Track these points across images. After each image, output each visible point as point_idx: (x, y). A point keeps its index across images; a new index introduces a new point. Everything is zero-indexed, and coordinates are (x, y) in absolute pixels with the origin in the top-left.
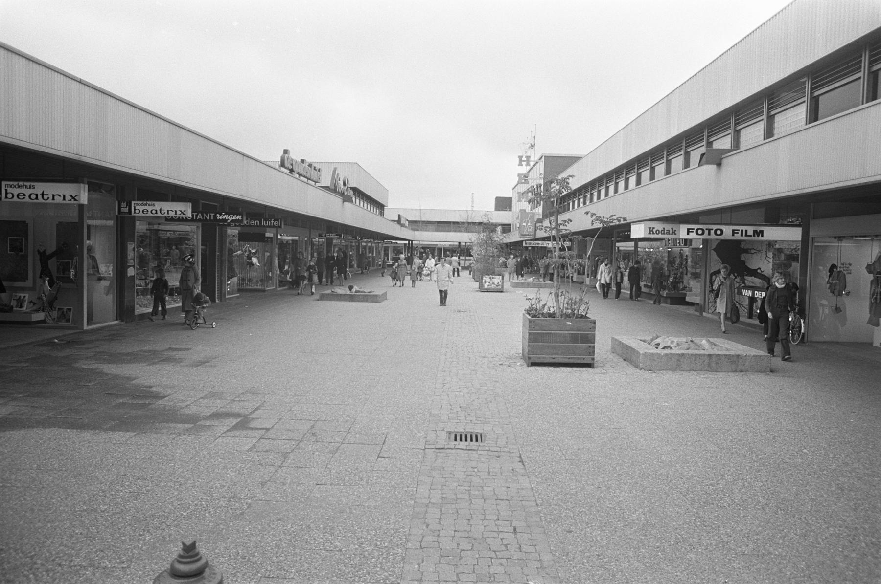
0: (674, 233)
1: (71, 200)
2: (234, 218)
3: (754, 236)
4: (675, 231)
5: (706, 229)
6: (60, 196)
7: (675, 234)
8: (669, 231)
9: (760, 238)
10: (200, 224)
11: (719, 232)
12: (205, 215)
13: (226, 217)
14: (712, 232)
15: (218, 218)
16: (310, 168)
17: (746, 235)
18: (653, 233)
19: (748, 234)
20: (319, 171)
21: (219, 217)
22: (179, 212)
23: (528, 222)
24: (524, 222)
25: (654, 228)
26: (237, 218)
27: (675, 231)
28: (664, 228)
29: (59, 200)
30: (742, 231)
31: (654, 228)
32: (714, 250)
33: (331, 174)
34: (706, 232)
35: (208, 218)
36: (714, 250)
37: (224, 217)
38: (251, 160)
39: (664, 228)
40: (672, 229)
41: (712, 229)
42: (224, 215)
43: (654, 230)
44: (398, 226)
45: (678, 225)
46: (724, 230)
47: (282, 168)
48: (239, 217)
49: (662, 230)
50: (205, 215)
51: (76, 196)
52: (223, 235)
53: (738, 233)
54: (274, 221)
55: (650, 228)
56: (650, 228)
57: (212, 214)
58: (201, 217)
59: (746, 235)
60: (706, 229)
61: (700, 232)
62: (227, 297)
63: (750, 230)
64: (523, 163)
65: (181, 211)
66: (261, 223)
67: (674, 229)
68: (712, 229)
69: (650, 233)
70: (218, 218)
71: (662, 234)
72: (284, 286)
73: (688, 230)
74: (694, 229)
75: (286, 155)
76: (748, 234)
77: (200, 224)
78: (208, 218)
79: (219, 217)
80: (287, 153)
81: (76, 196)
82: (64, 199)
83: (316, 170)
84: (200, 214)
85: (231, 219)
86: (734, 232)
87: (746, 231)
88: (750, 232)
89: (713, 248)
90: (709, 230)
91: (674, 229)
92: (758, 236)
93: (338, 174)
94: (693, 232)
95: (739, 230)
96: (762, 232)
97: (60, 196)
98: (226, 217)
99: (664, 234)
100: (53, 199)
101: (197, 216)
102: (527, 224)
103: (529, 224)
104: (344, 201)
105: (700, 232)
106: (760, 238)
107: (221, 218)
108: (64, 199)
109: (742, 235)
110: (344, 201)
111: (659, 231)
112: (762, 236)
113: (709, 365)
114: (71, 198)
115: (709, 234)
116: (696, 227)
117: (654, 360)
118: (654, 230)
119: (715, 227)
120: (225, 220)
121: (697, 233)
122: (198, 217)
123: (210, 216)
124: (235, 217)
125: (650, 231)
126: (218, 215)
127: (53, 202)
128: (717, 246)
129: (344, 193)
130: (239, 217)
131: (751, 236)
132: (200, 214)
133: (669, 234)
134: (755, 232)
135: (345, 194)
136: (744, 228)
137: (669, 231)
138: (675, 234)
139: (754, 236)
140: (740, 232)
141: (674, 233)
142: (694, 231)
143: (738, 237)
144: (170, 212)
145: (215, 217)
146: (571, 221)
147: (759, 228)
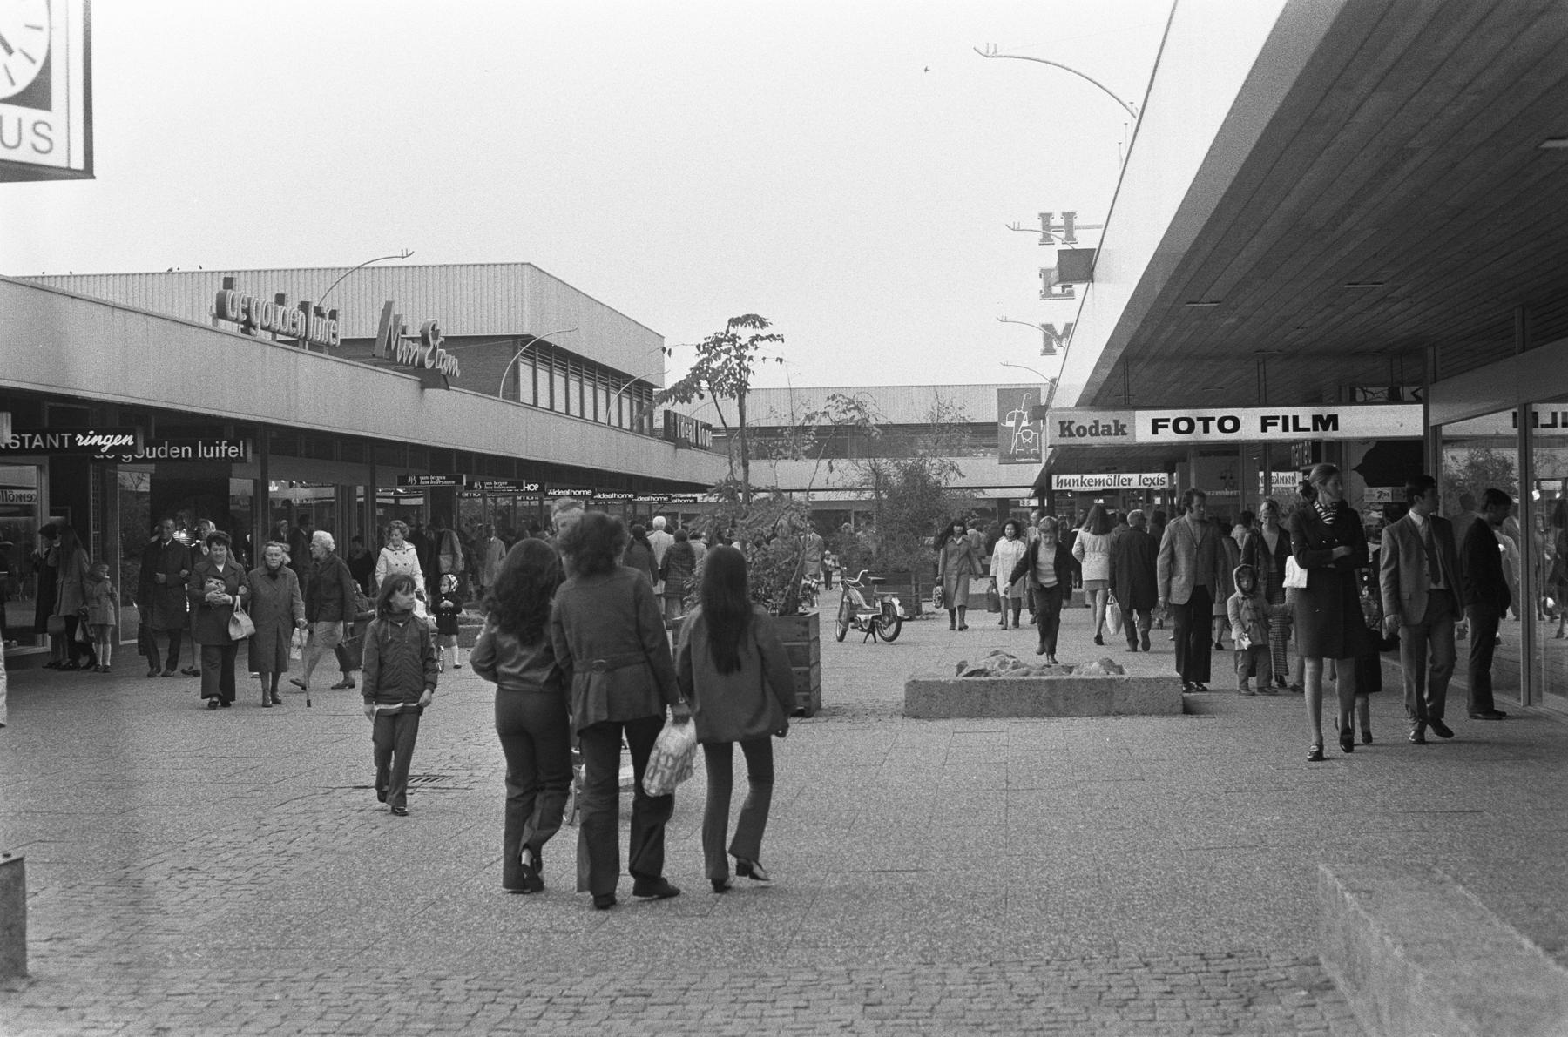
0: (1120, 430)
2: (116, 443)
4: (1124, 426)
5: (1199, 419)
8: (1109, 426)
10: (45, 460)
11: (1229, 425)
12: (49, 437)
13: (97, 440)
14: (1213, 425)
15: (80, 444)
16: (302, 314)
17: (1296, 428)
18: (1071, 435)
19: (1301, 425)
20: (333, 315)
21: (81, 441)
22: (292, 306)
23: (1021, 416)
24: (1011, 419)
25: (1071, 423)
26: (124, 442)
27: (1124, 426)
30: (1285, 419)
31: (1071, 423)
32: (1359, 469)
33: (378, 318)
34: (1199, 425)
35: (57, 445)
36: (1359, 469)
37: (93, 442)
39: (1096, 422)
40: (1116, 422)
41: (1213, 419)
42: (92, 436)
43: (1074, 428)
44: (665, 448)
46: (1242, 419)
47: (221, 321)
48: (128, 440)
49: (1091, 427)
50: (49, 437)
52: (108, 483)
53: (1275, 424)
54: (228, 445)
55: (1062, 423)
56: (1062, 423)
57: (27, 436)
58: (41, 443)
60: (1199, 419)
61: (1183, 426)
62: (121, 643)
63: (1305, 415)
64: (1061, 222)
66: (195, 451)
67: (1121, 422)
68: (1213, 419)
69: (1062, 435)
70: (80, 444)
71: (1092, 435)
73: (1155, 422)
74: (1168, 420)
75: (229, 291)
76: (1301, 425)
77: (45, 460)
78: (57, 445)
79: (81, 441)
80: (231, 288)
83: (323, 316)
84: (38, 436)
85: (109, 444)
86: (1156, 426)
87: (1296, 419)
88: (1306, 422)
89: (1354, 465)
90: (1206, 421)
91: (1121, 422)
92: (1325, 429)
93: (398, 318)
94: (1166, 427)
95: (1277, 418)
96: (1333, 419)
98: (97, 440)
99: (1097, 434)
101: (31, 440)
102: (1018, 423)
103: (1025, 423)
104: (424, 386)
105: (1183, 426)
107: (86, 443)
109: (1285, 429)
110: (424, 386)
111: (1084, 428)
112: (1335, 428)
113: (1050, 701)
115: (1206, 430)
116: (1172, 414)
117: (933, 696)
119: (1218, 413)
120: (97, 448)
121: (1176, 429)
122: (35, 443)
123: (62, 440)
124: (120, 440)
126: (79, 437)
128: (1366, 458)
129: (421, 364)
130: (128, 440)
131: (1307, 429)
132: (38, 436)
133: (1110, 434)
135: (428, 366)
136: (1290, 412)
139: (1315, 429)
140: (1280, 422)
142: (1170, 424)
143: (1275, 433)
145: (73, 441)
147: (1326, 411)
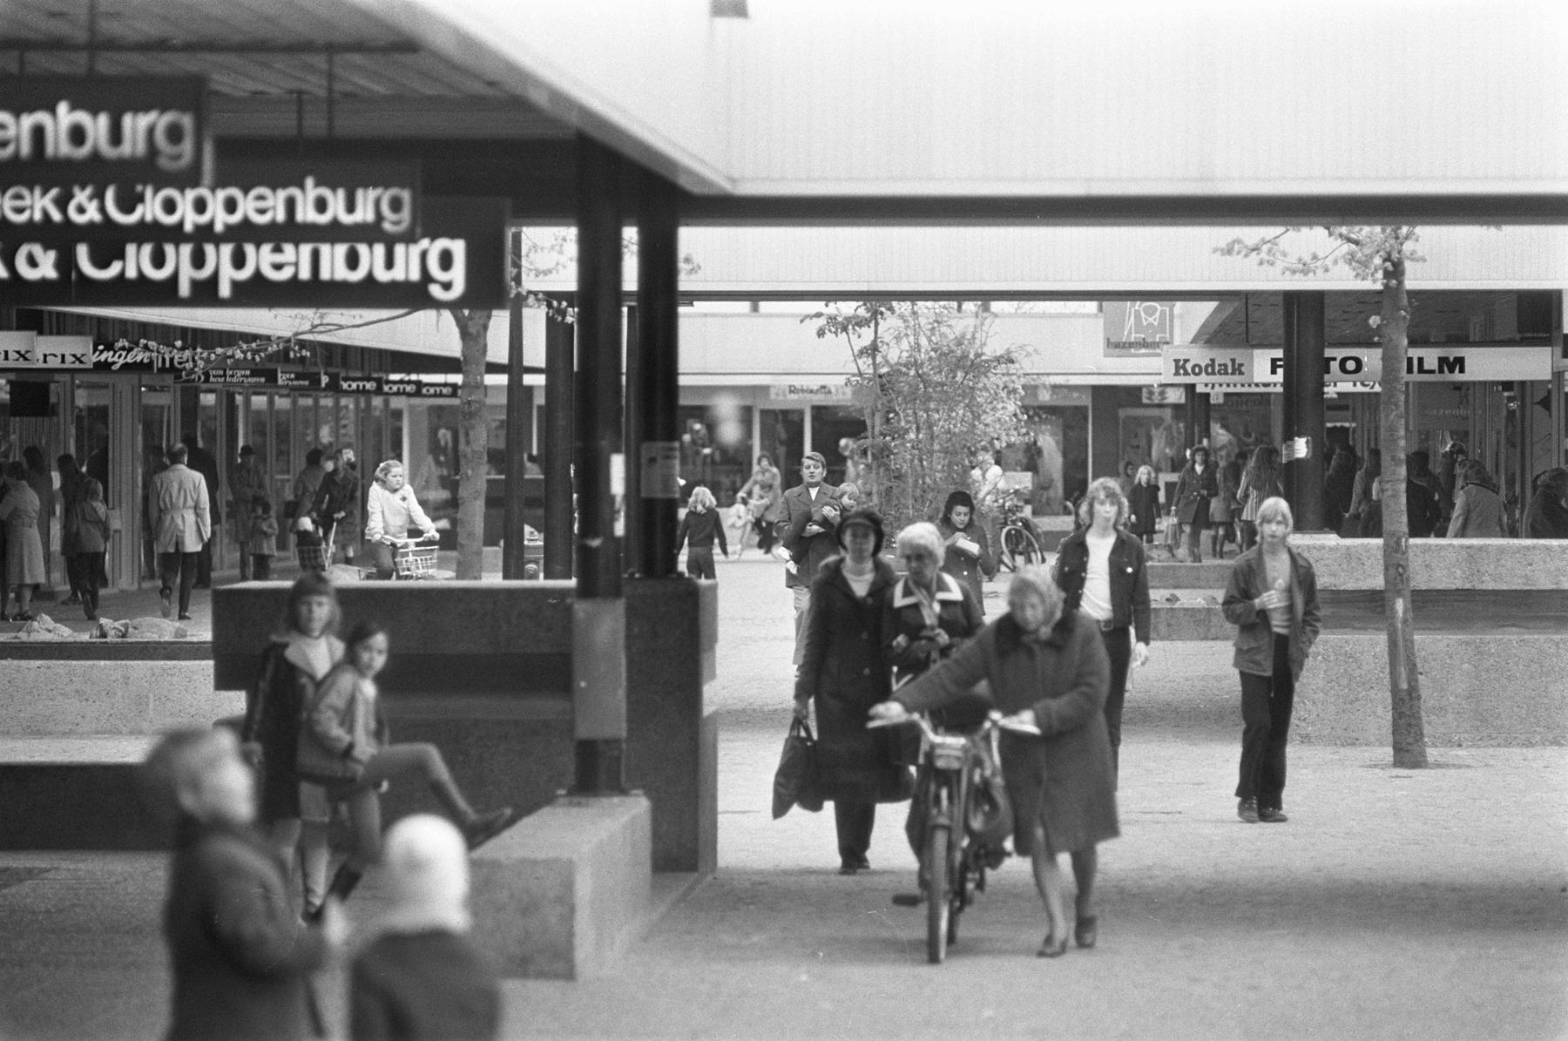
0: (1238, 369)
1: (74, 363)
2: (129, 360)
3: (1441, 371)
4: (1241, 365)
6: (55, 356)
7: (1241, 373)
8: (1225, 365)
9: (1457, 377)
11: (1351, 365)
17: (1421, 370)
18: (1186, 373)
19: (1426, 367)
25: (1186, 361)
27: (1241, 365)
28: (1213, 361)
29: (54, 363)
31: (1186, 361)
37: (103, 358)
38: (775, 320)
39: (1213, 361)
40: (1233, 361)
41: (1334, 359)
42: (101, 352)
43: (1189, 367)
45: (1249, 351)
49: (1207, 366)
51: (27, 352)
55: (1177, 361)
56: (1177, 361)
59: (1421, 370)
65: (74, 356)
68: (1334, 359)
69: (1177, 373)
71: (1207, 374)
72: (1134, 509)
76: (1426, 367)
81: (27, 352)
82: (63, 361)
85: (121, 361)
87: (1421, 360)
88: (1431, 362)
92: (1452, 371)
96: (1460, 361)
97: (55, 356)
99: (1213, 373)
100: (45, 361)
106: (1457, 377)
108: (63, 361)
112: (1462, 371)
114: (17, 356)
118: (1189, 367)
125: (1177, 368)
127: (45, 366)
131: (1432, 372)
133: (1226, 373)
134: (1443, 361)
137: (1225, 365)
138: (1241, 373)
139: (1441, 371)
141: (1238, 369)
144: (48, 358)
146: (859, 337)
147: (1453, 352)
